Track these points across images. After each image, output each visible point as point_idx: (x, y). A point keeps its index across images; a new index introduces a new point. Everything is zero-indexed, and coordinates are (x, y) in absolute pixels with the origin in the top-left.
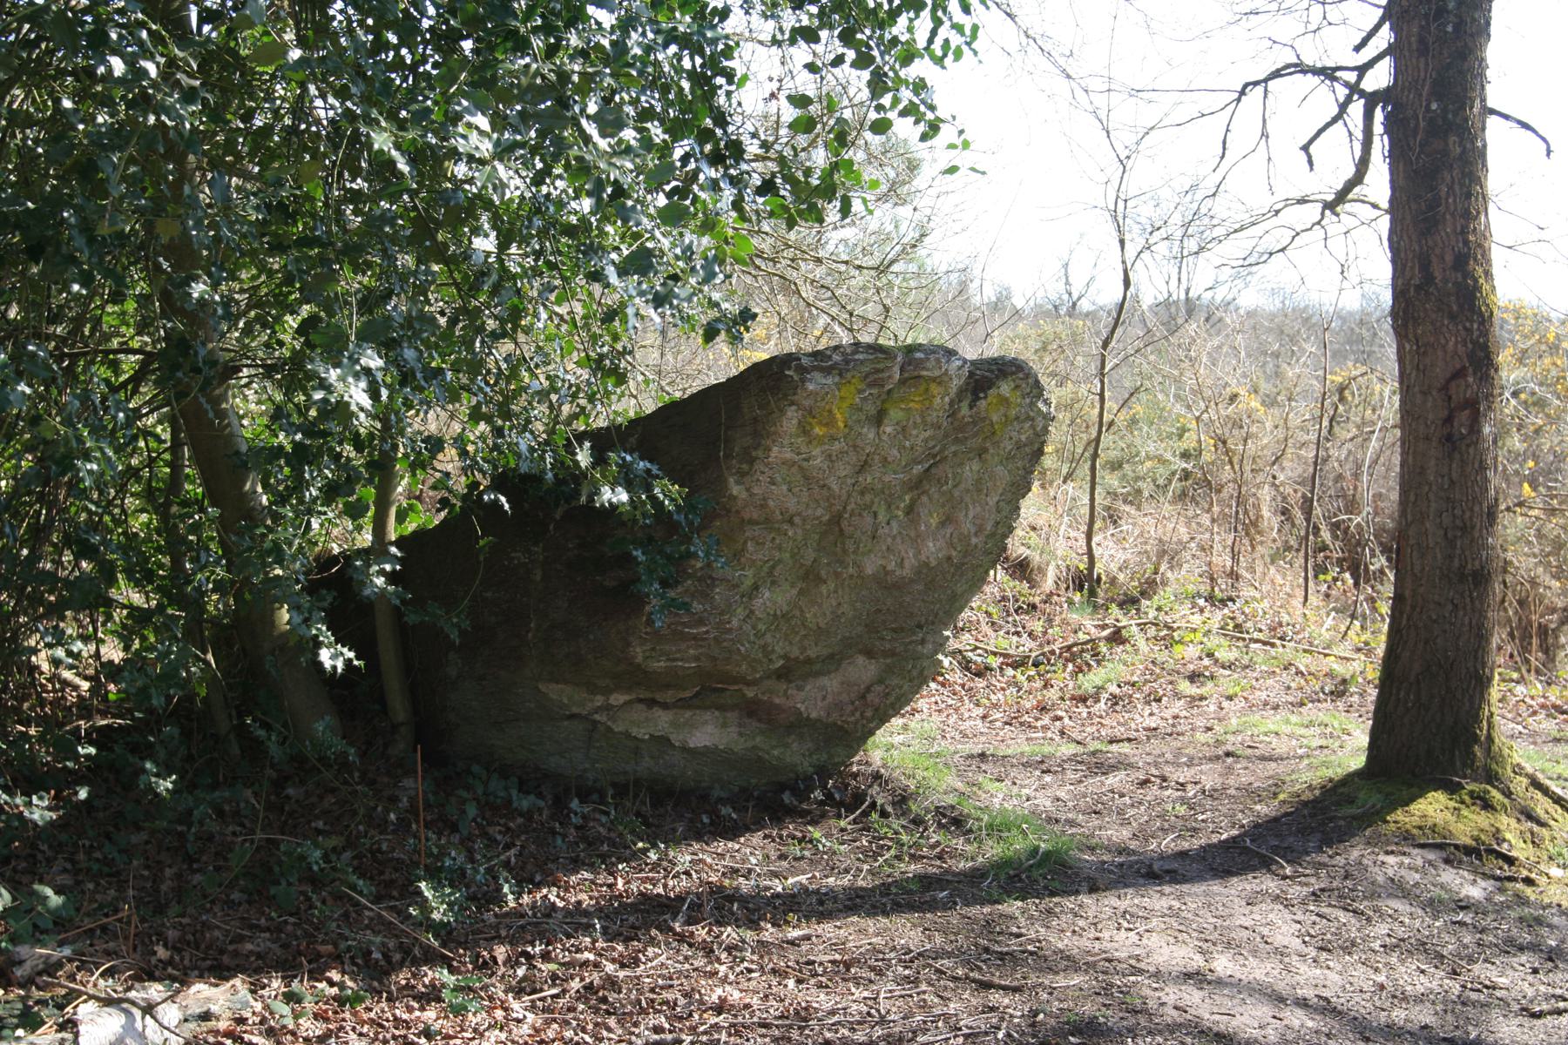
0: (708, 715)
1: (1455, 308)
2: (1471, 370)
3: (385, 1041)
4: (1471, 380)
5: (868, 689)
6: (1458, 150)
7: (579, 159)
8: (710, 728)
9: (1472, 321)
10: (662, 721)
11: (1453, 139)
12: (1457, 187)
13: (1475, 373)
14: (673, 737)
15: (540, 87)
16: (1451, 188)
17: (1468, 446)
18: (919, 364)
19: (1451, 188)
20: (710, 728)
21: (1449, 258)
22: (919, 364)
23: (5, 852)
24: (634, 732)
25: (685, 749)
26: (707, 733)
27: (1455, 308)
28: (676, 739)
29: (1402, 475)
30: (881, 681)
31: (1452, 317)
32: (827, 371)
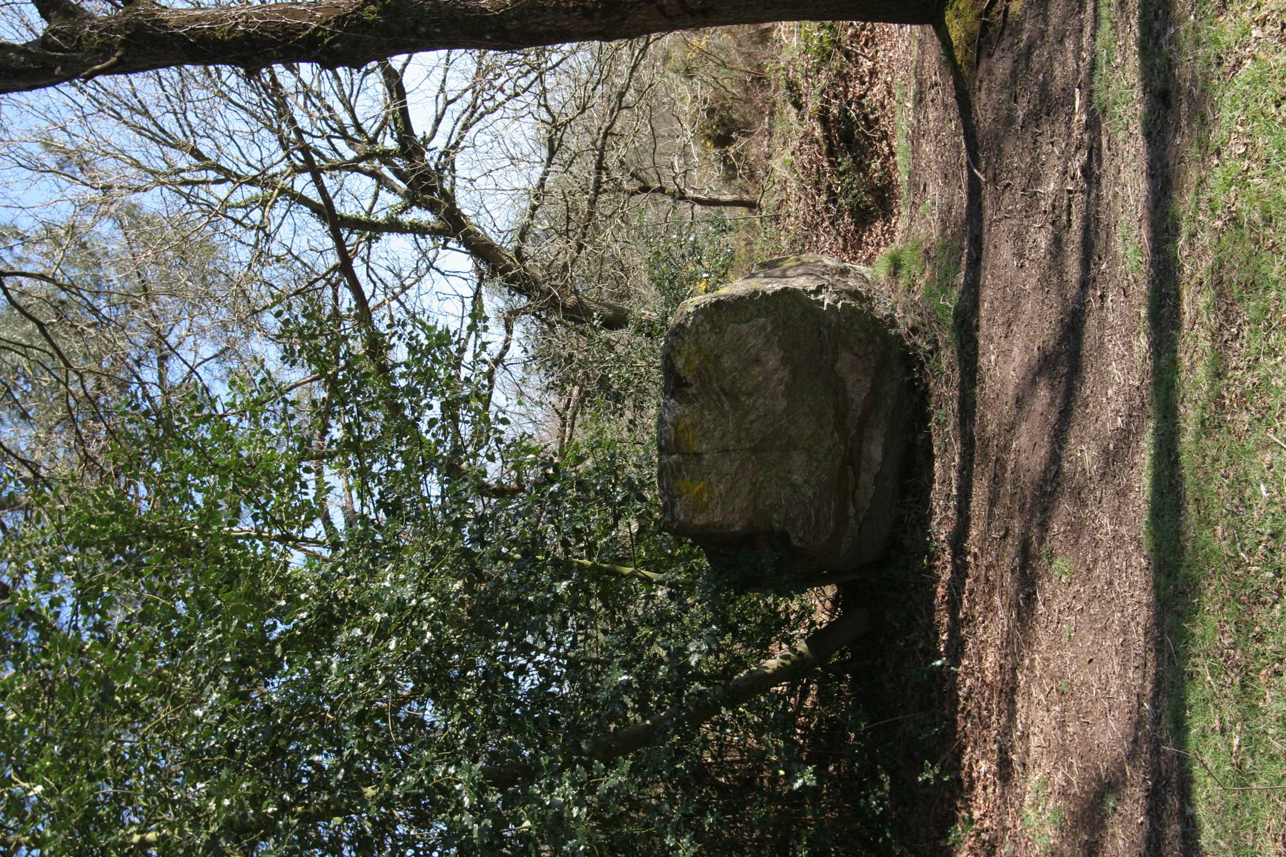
0: (865, 449)
1: (618, 17)
3: (334, 845)
5: (856, 354)
6: (515, 22)
8: (872, 448)
10: (866, 478)
11: (508, 26)
14: (875, 471)
16: (539, 24)
18: (667, 442)
19: (539, 24)
20: (872, 448)
21: (585, 22)
22: (667, 442)
23: (1230, 854)
24: (870, 496)
25: (883, 463)
26: (875, 450)
27: (618, 17)
30: (852, 348)
32: (673, 505)
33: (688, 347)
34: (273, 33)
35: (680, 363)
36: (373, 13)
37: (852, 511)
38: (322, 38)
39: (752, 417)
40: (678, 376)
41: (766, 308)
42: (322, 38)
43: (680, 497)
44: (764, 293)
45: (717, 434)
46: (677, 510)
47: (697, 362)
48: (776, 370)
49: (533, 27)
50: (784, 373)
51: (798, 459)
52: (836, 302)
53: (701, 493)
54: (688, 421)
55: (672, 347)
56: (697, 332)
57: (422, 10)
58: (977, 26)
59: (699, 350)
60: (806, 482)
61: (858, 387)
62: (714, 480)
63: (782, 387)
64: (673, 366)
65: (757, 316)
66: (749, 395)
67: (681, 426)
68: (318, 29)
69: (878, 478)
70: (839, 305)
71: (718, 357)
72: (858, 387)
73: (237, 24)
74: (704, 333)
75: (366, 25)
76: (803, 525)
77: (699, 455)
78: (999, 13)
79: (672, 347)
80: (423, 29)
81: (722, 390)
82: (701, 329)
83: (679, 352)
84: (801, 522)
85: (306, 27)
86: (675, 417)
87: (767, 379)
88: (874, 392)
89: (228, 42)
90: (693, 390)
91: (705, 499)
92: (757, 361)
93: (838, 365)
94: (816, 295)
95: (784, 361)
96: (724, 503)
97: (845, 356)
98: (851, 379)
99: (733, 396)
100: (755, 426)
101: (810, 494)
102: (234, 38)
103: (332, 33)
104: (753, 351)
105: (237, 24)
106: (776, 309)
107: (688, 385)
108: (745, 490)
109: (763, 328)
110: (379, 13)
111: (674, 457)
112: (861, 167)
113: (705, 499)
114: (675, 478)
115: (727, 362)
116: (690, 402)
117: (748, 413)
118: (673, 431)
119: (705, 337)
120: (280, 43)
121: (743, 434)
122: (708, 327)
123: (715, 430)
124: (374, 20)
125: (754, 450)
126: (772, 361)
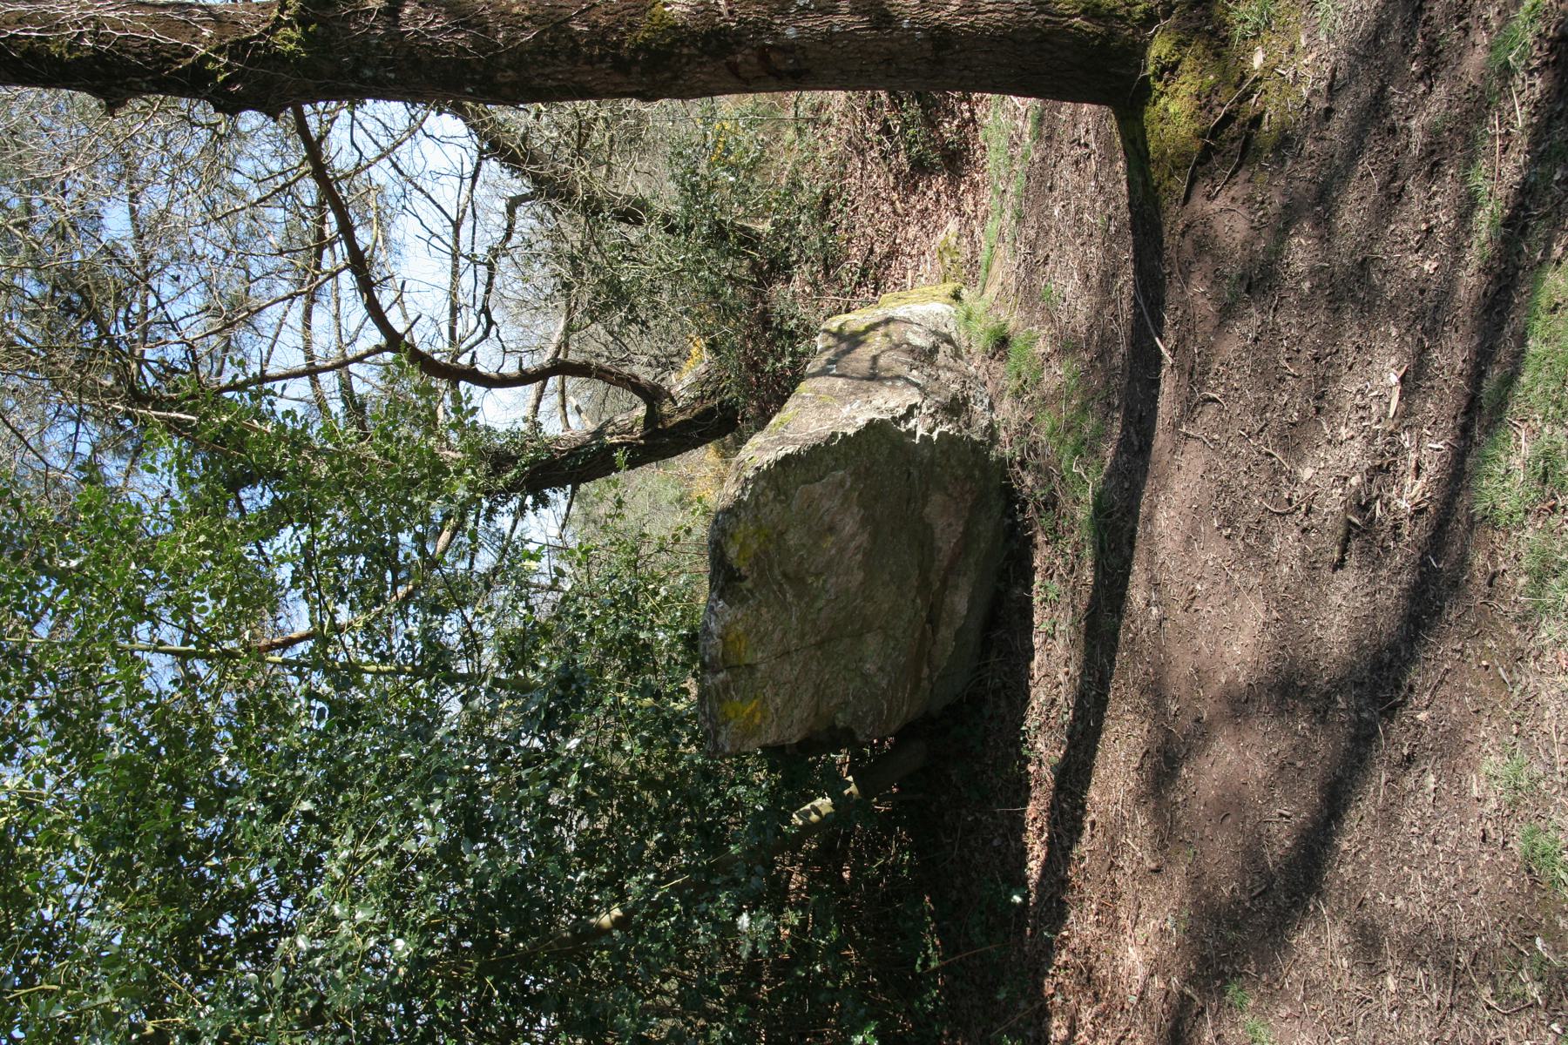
0: (948, 600)
1: (667, 75)
2: (730, 58)
4: (739, 58)
6: (510, 73)
7: (162, 362)
8: (957, 599)
9: (681, 55)
10: (945, 633)
12: (548, 71)
13: (733, 53)
15: (818, 823)
16: (548, 77)
17: (806, 58)
19: (548, 77)
20: (957, 599)
21: (618, 79)
26: (960, 602)
27: (667, 75)
28: (959, 623)
29: (1028, 627)
30: (946, 489)
31: (676, 78)
32: (717, 733)
33: (744, 528)
34: (139, 56)
35: (732, 551)
36: (291, 40)
37: (926, 671)
38: (215, 73)
39: (820, 603)
40: (730, 568)
41: (846, 454)
42: (215, 73)
43: (726, 724)
44: (844, 435)
45: (777, 636)
46: (721, 739)
47: (755, 546)
48: (853, 536)
49: (537, 81)
50: (863, 539)
51: (872, 643)
52: (931, 431)
53: (753, 714)
54: (740, 628)
55: (723, 531)
56: (757, 504)
57: (366, 43)
58: (1196, 147)
59: (760, 528)
60: (881, 669)
61: (946, 528)
62: (769, 694)
63: (859, 557)
64: (723, 555)
65: (834, 469)
66: (818, 575)
67: (732, 636)
68: (205, 58)
69: (958, 634)
70: (935, 436)
71: (781, 534)
72: (946, 528)
73: (81, 35)
74: (765, 505)
75: (280, 58)
76: (872, 723)
77: (751, 668)
78: (1233, 140)
79: (723, 531)
80: (368, 73)
81: (785, 575)
82: (762, 499)
83: (732, 535)
84: (870, 719)
85: (188, 52)
86: (724, 627)
87: (842, 551)
88: (968, 537)
89: (69, 63)
90: (748, 584)
91: (757, 721)
92: (831, 529)
93: (927, 510)
94: (907, 422)
95: (864, 522)
96: (780, 718)
97: (937, 498)
98: (940, 524)
99: (797, 579)
100: (823, 615)
101: (884, 684)
102: (79, 59)
103: (227, 67)
104: (827, 519)
105: (81, 35)
106: (858, 453)
107: (742, 578)
108: (806, 697)
109: (841, 484)
110: (299, 42)
111: (721, 676)
112: (933, 124)
113: (757, 721)
114: (721, 701)
115: (792, 539)
116: (744, 600)
117: (815, 598)
118: (720, 646)
119: (767, 510)
120: (150, 73)
121: (807, 629)
122: (771, 495)
123: (774, 631)
124: (291, 52)
125: (819, 645)
126: (849, 525)
